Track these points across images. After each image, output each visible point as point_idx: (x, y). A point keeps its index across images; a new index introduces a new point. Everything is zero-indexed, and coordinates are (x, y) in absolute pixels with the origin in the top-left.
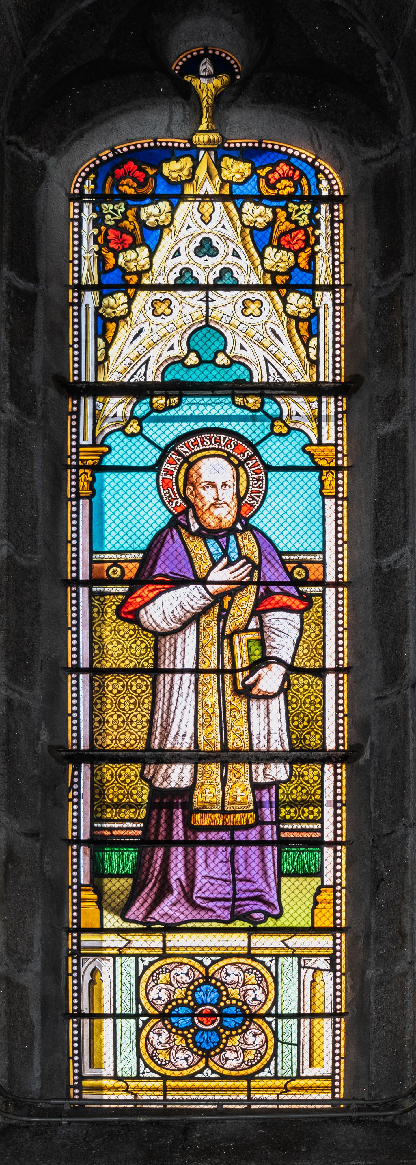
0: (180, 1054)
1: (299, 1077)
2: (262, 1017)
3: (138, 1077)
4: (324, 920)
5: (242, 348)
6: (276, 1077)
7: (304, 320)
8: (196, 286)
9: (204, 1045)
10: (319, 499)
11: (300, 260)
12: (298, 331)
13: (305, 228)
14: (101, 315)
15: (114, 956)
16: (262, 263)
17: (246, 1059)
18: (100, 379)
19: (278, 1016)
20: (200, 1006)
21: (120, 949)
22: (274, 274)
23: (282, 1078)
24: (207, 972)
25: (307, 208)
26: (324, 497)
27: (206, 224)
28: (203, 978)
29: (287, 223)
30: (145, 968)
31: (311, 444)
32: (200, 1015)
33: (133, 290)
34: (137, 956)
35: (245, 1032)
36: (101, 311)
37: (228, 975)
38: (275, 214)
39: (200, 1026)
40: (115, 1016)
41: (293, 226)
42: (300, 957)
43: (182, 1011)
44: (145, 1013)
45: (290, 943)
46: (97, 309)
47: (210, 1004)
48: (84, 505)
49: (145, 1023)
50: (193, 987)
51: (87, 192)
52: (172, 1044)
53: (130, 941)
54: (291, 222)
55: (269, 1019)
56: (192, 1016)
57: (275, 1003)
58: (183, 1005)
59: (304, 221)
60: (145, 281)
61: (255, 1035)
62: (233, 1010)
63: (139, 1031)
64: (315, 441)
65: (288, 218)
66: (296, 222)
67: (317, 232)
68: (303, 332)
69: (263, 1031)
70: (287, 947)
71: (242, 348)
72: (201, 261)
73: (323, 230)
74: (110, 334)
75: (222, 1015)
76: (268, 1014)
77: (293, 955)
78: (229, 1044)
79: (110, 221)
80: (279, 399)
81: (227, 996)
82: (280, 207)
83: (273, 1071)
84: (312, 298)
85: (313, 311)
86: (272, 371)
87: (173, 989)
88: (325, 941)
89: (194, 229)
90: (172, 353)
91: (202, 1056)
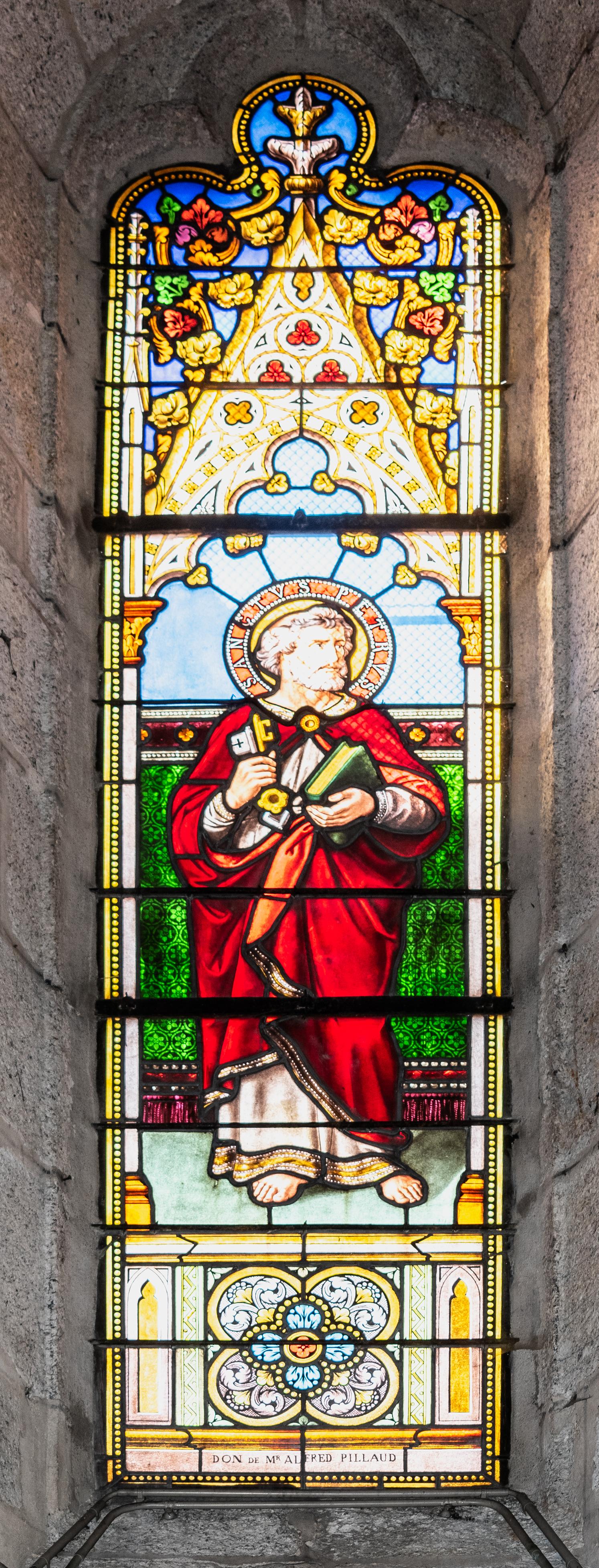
0: (265, 1398)
1: (433, 1426)
2: (382, 1344)
3: (206, 1426)
4: (471, 1214)
5: (350, 468)
6: (401, 1426)
7: (439, 431)
8: (289, 384)
9: (300, 1385)
10: (460, 669)
11: (437, 348)
12: (432, 446)
13: (443, 305)
14: (152, 425)
15: (174, 1265)
16: (383, 354)
17: (358, 1403)
18: (150, 511)
19: (403, 1343)
20: (292, 1331)
21: (180, 1256)
22: (398, 368)
23: (410, 1427)
24: (304, 1287)
25: (447, 279)
26: (465, 666)
27: (303, 301)
28: (298, 1296)
29: (421, 299)
30: (217, 1282)
31: (448, 596)
32: (296, 1342)
33: (197, 390)
34: (207, 1266)
35: (356, 1366)
36: (151, 419)
37: (332, 1289)
38: (401, 287)
39: (293, 1359)
40: (174, 1344)
41: (428, 303)
42: (434, 1264)
43: (268, 1337)
44: (216, 1341)
45: (421, 1246)
46: (146, 414)
47: (310, 1330)
48: (130, 674)
49: (216, 1354)
50: (286, 1308)
51: (133, 261)
52: (254, 1384)
53: (195, 1244)
54: (426, 297)
55: (390, 1347)
56: (281, 1343)
57: (400, 1327)
58: (269, 1331)
59: (442, 296)
60: (216, 377)
61: (371, 1371)
62: (338, 1336)
63: (208, 1365)
64: (454, 592)
65: (422, 293)
66: (431, 298)
67: (460, 309)
68: (439, 447)
69: (382, 1365)
70: (420, 1252)
71: (350, 468)
72: (294, 350)
73: (470, 309)
74: (164, 448)
75: (324, 1343)
76: (392, 1341)
77: (427, 1261)
78: (334, 1383)
79: (165, 299)
80: (401, 538)
81: (332, 1318)
82: (409, 277)
83: (397, 1419)
84: (453, 396)
85: (454, 417)
86: (391, 497)
87: (256, 1310)
88: (473, 1244)
89: (286, 309)
90: (252, 476)
91: (297, 1399)
